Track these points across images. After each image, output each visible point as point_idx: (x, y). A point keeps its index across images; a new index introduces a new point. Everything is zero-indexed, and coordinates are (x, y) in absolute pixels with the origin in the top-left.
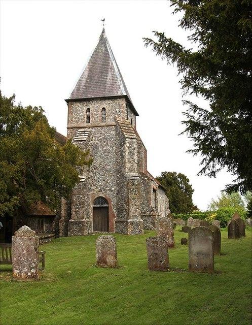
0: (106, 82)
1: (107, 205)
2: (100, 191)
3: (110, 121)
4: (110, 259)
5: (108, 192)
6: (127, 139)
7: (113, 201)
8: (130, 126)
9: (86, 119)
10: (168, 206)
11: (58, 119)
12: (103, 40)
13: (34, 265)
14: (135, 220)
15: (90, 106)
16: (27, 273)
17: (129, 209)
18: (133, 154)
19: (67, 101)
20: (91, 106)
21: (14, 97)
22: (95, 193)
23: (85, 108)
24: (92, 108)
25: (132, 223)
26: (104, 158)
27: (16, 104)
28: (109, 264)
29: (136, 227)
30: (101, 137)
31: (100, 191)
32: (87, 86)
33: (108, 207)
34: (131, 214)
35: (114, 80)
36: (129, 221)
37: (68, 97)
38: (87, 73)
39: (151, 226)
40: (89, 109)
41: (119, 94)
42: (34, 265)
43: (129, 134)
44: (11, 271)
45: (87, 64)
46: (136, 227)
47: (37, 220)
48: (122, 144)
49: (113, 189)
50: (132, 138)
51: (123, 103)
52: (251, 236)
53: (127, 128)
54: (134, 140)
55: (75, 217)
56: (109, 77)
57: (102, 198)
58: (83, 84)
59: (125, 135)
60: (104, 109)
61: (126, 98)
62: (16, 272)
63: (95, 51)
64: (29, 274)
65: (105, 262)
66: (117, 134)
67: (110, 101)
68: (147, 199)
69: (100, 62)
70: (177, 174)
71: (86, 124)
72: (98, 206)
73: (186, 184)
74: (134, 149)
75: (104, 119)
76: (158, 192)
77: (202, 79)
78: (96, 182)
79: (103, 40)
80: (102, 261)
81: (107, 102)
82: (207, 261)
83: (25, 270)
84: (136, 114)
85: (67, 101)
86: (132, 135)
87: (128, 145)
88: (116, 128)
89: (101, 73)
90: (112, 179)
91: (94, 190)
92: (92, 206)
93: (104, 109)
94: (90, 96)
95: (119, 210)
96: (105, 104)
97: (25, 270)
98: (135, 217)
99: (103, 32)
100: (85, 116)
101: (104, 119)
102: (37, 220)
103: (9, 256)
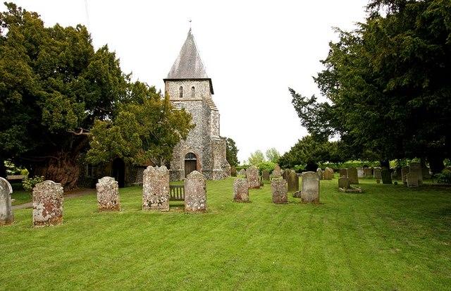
3: (198, 97)
4: (244, 196)
7: (200, 156)
11: (160, 87)
12: (190, 36)
13: (203, 201)
15: (183, 85)
16: (197, 207)
19: (165, 80)
20: (184, 84)
21: (131, 74)
23: (179, 87)
25: (216, 172)
26: (197, 119)
27: (365, 22)
28: (243, 199)
32: (180, 71)
35: (201, 66)
37: (166, 77)
38: (179, 60)
42: (203, 201)
44: (184, 206)
45: (179, 53)
51: (207, 83)
56: (197, 64)
58: (177, 68)
59: (209, 109)
60: (193, 87)
61: (210, 80)
62: (188, 206)
63: (185, 44)
64: (199, 208)
65: (241, 199)
66: (204, 107)
67: (198, 82)
69: (189, 53)
71: (179, 99)
73: (233, 146)
75: (193, 95)
78: (191, 143)
79: (190, 36)
80: (238, 198)
81: (195, 82)
82: (314, 196)
83: (196, 205)
84: (213, 93)
85: (165, 80)
87: (212, 115)
88: (203, 103)
90: (199, 140)
92: (184, 159)
94: (182, 77)
95: (204, 162)
96: (194, 84)
97: (196, 205)
98: (218, 167)
99: (293, 92)
101: (193, 95)
103: (182, 193)
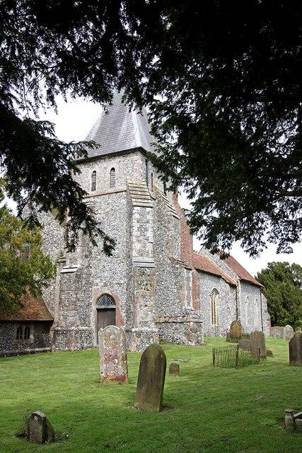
0: (118, 134)
1: (114, 307)
2: (105, 285)
3: (119, 187)
5: (116, 287)
6: (136, 208)
8: (147, 190)
9: (91, 186)
10: (266, 308)
14: (145, 329)
17: (135, 312)
18: (146, 230)
22: (98, 289)
23: (91, 172)
24: (98, 171)
25: (139, 334)
29: (145, 340)
30: (108, 209)
31: (105, 285)
33: (114, 310)
34: (138, 319)
36: (133, 330)
39: (184, 338)
40: (95, 172)
41: (132, 147)
43: (140, 200)
46: (145, 340)
47: (16, 327)
48: (130, 215)
49: (122, 282)
50: (143, 207)
52: (137, 374)
53: (140, 193)
54: (148, 209)
55: (63, 324)
56: (124, 126)
57: (108, 295)
60: (113, 169)
68: (178, 298)
70: (291, 265)
72: (103, 307)
74: (148, 222)
75: (112, 184)
76: (239, 287)
77: (31, 20)
86: (146, 201)
89: (115, 123)
91: (97, 285)
92: (94, 307)
93: (113, 169)
96: (114, 163)
100: (91, 182)
101: (112, 184)
102: (16, 327)
